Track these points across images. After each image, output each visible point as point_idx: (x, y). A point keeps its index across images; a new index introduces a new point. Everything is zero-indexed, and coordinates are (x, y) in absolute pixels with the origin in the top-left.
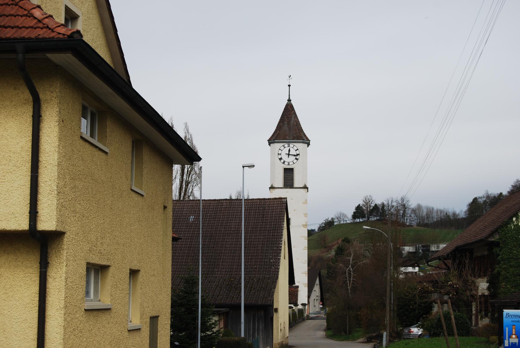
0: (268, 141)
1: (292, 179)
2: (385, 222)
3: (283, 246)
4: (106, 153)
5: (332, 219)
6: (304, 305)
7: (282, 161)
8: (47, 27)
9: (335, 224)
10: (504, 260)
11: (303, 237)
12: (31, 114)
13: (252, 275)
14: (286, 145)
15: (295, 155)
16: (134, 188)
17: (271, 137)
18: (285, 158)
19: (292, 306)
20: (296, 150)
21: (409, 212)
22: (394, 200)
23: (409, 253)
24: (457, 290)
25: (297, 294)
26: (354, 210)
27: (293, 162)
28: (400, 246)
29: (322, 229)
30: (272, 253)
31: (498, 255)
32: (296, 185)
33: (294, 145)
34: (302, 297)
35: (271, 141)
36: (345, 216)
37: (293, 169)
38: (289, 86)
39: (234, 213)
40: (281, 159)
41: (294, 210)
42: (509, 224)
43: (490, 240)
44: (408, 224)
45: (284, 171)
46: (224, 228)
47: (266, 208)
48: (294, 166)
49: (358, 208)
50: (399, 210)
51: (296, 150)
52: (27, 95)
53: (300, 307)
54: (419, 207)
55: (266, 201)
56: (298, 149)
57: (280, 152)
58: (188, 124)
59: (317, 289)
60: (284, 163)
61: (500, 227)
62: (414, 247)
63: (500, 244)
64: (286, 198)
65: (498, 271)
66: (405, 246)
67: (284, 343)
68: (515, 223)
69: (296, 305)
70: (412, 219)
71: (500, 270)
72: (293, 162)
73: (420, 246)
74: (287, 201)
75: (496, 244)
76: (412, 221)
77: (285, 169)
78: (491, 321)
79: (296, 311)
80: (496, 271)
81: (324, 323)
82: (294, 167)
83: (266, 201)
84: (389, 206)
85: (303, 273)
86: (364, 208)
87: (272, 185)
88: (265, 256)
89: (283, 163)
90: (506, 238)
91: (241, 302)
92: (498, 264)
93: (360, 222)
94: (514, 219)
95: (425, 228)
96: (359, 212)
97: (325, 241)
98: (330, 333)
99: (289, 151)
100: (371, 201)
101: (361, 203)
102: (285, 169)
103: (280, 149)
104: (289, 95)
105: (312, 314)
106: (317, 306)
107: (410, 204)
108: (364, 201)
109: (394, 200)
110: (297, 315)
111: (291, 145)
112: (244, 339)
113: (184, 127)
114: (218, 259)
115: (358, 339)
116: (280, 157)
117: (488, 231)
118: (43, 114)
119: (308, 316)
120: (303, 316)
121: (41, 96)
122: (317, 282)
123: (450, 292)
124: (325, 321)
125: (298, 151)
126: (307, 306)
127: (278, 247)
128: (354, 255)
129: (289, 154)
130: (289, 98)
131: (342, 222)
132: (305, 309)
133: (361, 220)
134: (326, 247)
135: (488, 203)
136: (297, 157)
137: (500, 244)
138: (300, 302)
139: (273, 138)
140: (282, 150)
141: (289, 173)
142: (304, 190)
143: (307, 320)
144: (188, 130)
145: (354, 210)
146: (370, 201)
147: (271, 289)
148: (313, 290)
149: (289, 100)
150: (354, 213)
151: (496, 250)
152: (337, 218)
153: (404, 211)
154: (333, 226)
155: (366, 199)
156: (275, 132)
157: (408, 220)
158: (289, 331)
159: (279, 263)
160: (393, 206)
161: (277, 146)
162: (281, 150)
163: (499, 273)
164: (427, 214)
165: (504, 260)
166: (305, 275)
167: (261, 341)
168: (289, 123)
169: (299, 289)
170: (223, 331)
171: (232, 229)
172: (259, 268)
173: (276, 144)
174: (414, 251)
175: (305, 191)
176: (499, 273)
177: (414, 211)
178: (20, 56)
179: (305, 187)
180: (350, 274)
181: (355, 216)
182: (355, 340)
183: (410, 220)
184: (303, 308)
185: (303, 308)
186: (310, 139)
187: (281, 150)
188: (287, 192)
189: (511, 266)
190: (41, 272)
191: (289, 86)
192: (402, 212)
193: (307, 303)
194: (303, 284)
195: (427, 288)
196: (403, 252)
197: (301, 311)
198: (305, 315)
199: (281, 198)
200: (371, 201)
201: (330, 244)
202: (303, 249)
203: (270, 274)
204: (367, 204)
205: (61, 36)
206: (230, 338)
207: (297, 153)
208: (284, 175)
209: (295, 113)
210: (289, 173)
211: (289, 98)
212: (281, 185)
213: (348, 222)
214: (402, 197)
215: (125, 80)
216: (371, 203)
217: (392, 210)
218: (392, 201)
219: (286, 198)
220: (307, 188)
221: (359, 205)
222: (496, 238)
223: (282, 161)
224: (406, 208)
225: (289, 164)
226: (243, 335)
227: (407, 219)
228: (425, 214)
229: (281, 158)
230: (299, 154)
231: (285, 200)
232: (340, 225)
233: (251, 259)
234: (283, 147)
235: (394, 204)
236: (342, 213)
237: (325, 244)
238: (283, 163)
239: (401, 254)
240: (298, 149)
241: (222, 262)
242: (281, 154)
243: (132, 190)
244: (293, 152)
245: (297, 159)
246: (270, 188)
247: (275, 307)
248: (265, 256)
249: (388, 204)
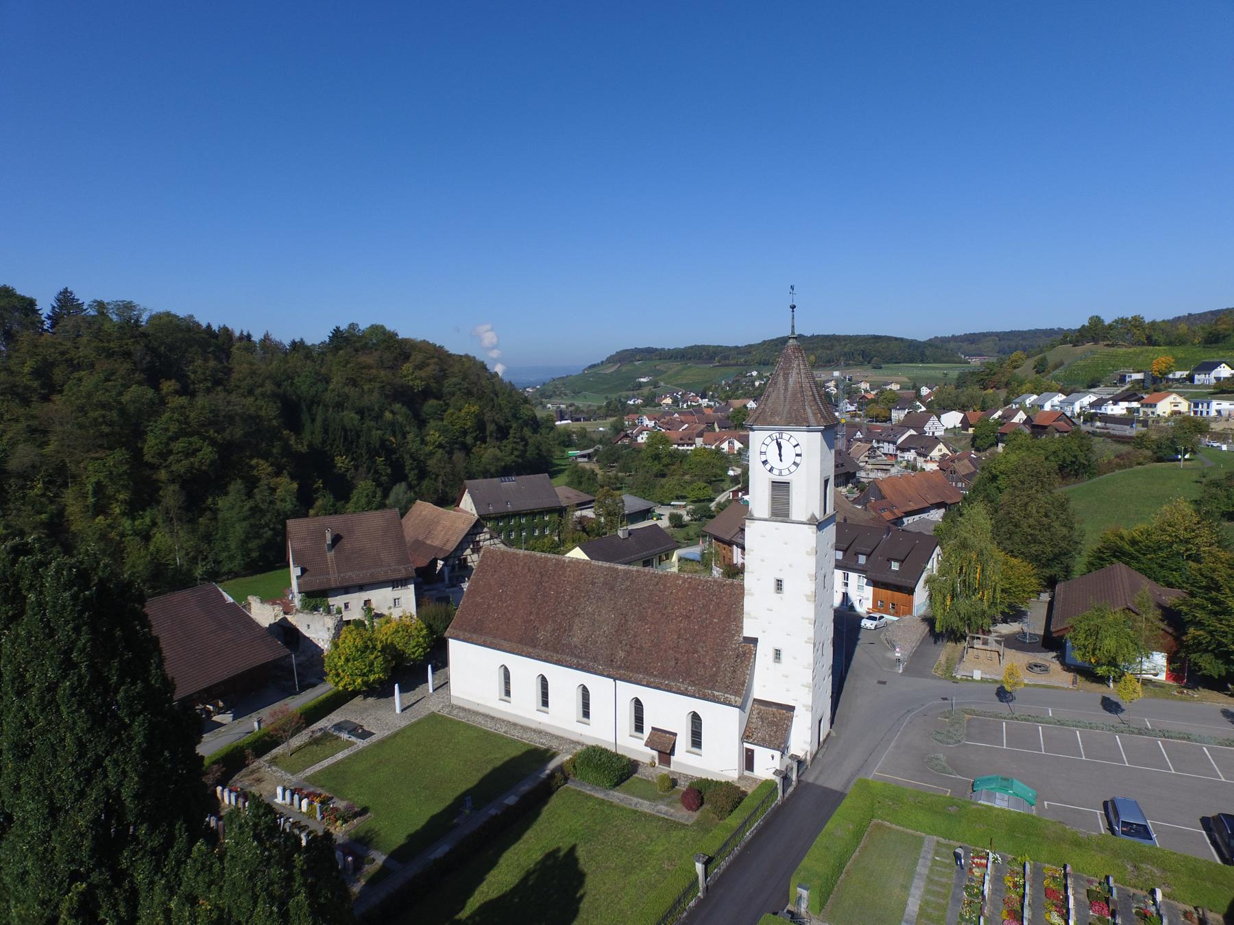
7: (768, 467)
11: (805, 619)
20: (795, 446)
32: (795, 515)
38: (793, 307)
40: (765, 462)
42: (162, 844)
45: (773, 486)
51: (795, 446)
56: (798, 445)
60: (771, 470)
78: (585, 747)
89: (770, 471)
111: (786, 436)
135: (108, 880)
188: (777, 529)
191: (793, 307)
202: (806, 642)
208: (772, 494)
212: (766, 515)
215: (484, 887)
223: (768, 467)
225: (780, 474)
229: (766, 461)
234: (769, 439)
238: (770, 471)
240: (798, 445)
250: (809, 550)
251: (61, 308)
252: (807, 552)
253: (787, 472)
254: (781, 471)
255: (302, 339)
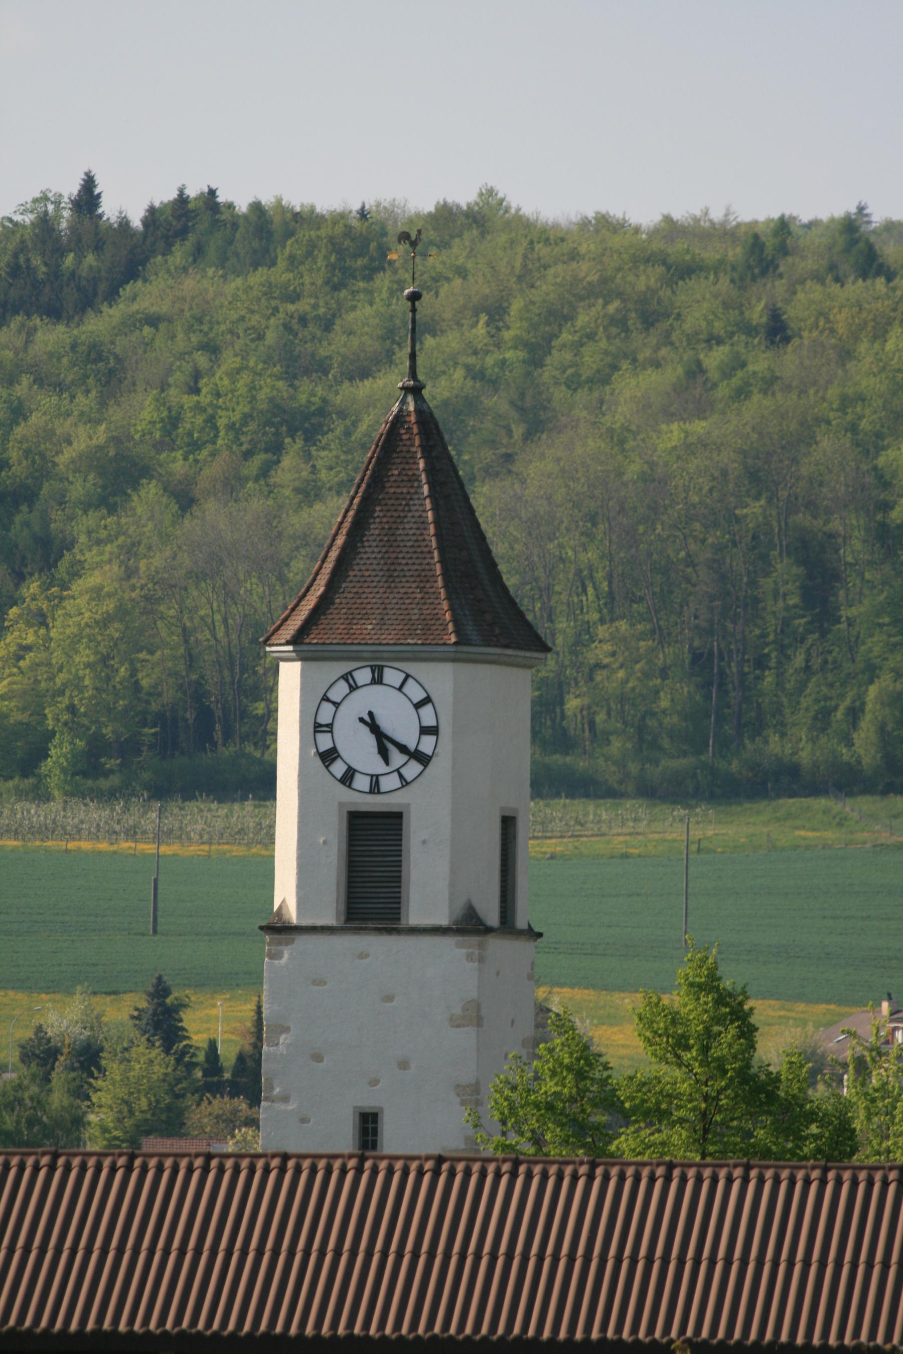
7: (339, 769)
27: (401, 776)
33: (408, 676)
37: (398, 816)
48: (405, 801)
60: (348, 778)
72: (401, 776)
82: (408, 805)
103: (325, 699)
125: (432, 739)
140: (337, 705)
142: (459, 945)
162: (334, 703)
170: (371, 524)
175: (464, 951)
187: (334, 703)
207: (421, 748)
223: (339, 769)
225: (375, 788)
234: (342, 688)
240: (427, 700)
242: (330, 726)
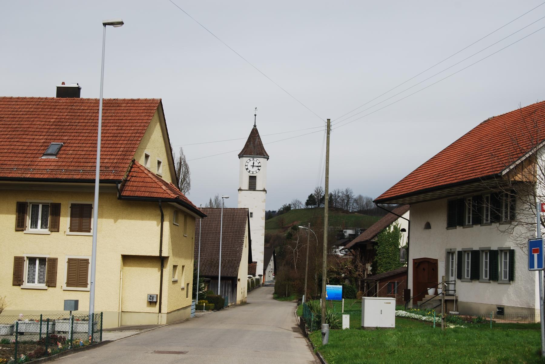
0: (238, 155)
1: (255, 184)
2: (331, 209)
3: (245, 240)
4: (178, 226)
5: (290, 205)
6: (260, 276)
7: (248, 171)
8: (168, 193)
9: (292, 209)
10: (380, 254)
12: (160, 219)
13: (225, 258)
14: (252, 159)
15: (257, 166)
16: (175, 223)
17: (241, 153)
18: (250, 168)
19: (251, 276)
21: (352, 201)
22: (340, 191)
23: (350, 235)
24: (350, 272)
25: (256, 268)
26: (307, 199)
28: (344, 229)
29: (281, 212)
30: (238, 244)
31: (377, 250)
32: (257, 188)
34: (259, 270)
35: (241, 156)
36: (300, 203)
38: (255, 115)
39: (214, 217)
40: (247, 169)
41: (256, 207)
43: (372, 241)
44: (350, 211)
46: (208, 227)
47: (235, 215)
49: (311, 197)
50: (343, 200)
52: (159, 212)
53: (257, 277)
54: (360, 197)
55: (235, 210)
57: (247, 164)
58: (183, 149)
59: (271, 264)
60: (249, 172)
61: (379, 233)
62: (354, 230)
63: (378, 243)
64: (248, 209)
65: (376, 260)
66: (347, 229)
67: (244, 301)
68: (388, 231)
69: (254, 275)
70: (354, 207)
71: (378, 259)
73: (359, 229)
74: (248, 210)
75: (375, 244)
76: (354, 209)
77: (250, 176)
79: (254, 279)
80: (375, 260)
81: (273, 289)
83: (235, 210)
84: (335, 196)
85: (260, 253)
86: (316, 197)
87: (240, 188)
88: (234, 246)
90: (382, 240)
91: (99, 203)
92: (376, 256)
93: (312, 208)
94: (387, 228)
95: (364, 215)
96: (311, 200)
97: (283, 223)
98: (276, 296)
99: (254, 163)
100: (322, 191)
101: (313, 192)
102: (250, 176)
104: (255, 122)
105: (267, 282)
106: (271, 276)
107: (353, 195)
108: (315, 191)
109: (340, 191)
110: (255, 283)
111: (255, 159)
112: (221, 296)
113: (180, 150)
114: (204, 247)
115: (293, 300)
116: (246, 167)
117: (370, 237)
118: (164, 219)
119: (263, 284)
120: (259, 284)
121: (164, 213)
122: (272, 258)
123: (346, 272)
124: (274, 287)
126: (262, 277)
127: (241, 241)
128: (299, 240)
129: (253, 166)
130: (255, 124)
131: (297, 208)
132: (261, 279)
133: (313, 207)
134: (283, 228)
136: (259, 168)
137: (378, 243)
138: (257, 274)
139: (242, 154)
141: (253, 179)
143: (262, 286)
144: (182, 153)
145: (307, 198)
146: (320, 192)
147: (236, 267)
148: (269, 264)
149: (255, 126)
150: (307, 200)
151: (376, 247)
152: (294, 204)
153: (348, 201)
154: (290, 211)
155: (317, 190)
156: (243, 149)
157: (351, 208)
158: (248, 294)
159: (242, 251)
160: (339, 196)
161: (245, 159)
163: (377, 261)
164: (366, 204)
165: (380, 254)
166: (262, 254)
167: (229, 298)
168: (254, 143)
169: (257, 264)
171: (213, 228)
172: (229, 254)
173: (244, 158)
174: (354, 234)
176: (377, 261)
177: (356, 201)
178: (160, 203)
179: (264, 190)
180: (296, 253)
181: (308, 203)
182: (291, 301)
183: (352, 208)
184: (259, 278)
185: (259, 278)
186: (269, 155)
188: (251, 193)
189: (384, 257)
190: (161, 269)
191: (255, 115)
192: (346, 201)
193: (263, 275)
194: (261, 261)
195: (332, 269)
196: (345, 234)
197: (258, 280)
198: (261, 283)
199: (245, 209)
200: (322, 191)
201: (286, 226)
203: (236, 258)
204: (318, 193)
205: (173, 198)
206: (212, 295)
209: (259, 136)
210: (253, 179)
211: (255, 124)
212: (247, 188)
213: (302, 208)
214: (346, 189)
216: (322, 193)
217: (338, 199)
218: (338, 192)
219: (248, 209)
220: (266, 191)
221: (312, 194)
222: (376, 239)
223: (248, 171)
224: (349, 198)
225: (253, 173)
226: (219, 294)
227: (350, 207)
228: (365, 203)
230: (260, 166)
231: (247, 210)
232: (296, 210)
233: (225, 247)
235: (340, 194)
236: (297, 200)
237: (282, 225)
239: (343, 235)
241: (206, 249)
243: (174, 224)
244: (256, 164)
245: (259, 169)
246: (239, 190)
247: (238, 278)
248: (234, 246)
249: (335, 194)
250: (263, 200)
251: (30, 342)
252: (293, 328)
253: (255, 172)
254: (253, 172)
255: (256, 262)
